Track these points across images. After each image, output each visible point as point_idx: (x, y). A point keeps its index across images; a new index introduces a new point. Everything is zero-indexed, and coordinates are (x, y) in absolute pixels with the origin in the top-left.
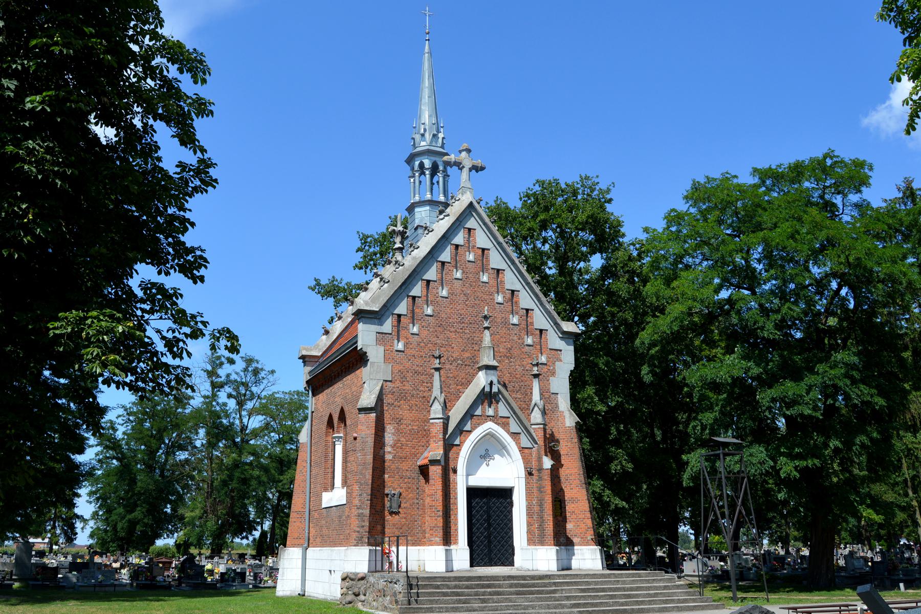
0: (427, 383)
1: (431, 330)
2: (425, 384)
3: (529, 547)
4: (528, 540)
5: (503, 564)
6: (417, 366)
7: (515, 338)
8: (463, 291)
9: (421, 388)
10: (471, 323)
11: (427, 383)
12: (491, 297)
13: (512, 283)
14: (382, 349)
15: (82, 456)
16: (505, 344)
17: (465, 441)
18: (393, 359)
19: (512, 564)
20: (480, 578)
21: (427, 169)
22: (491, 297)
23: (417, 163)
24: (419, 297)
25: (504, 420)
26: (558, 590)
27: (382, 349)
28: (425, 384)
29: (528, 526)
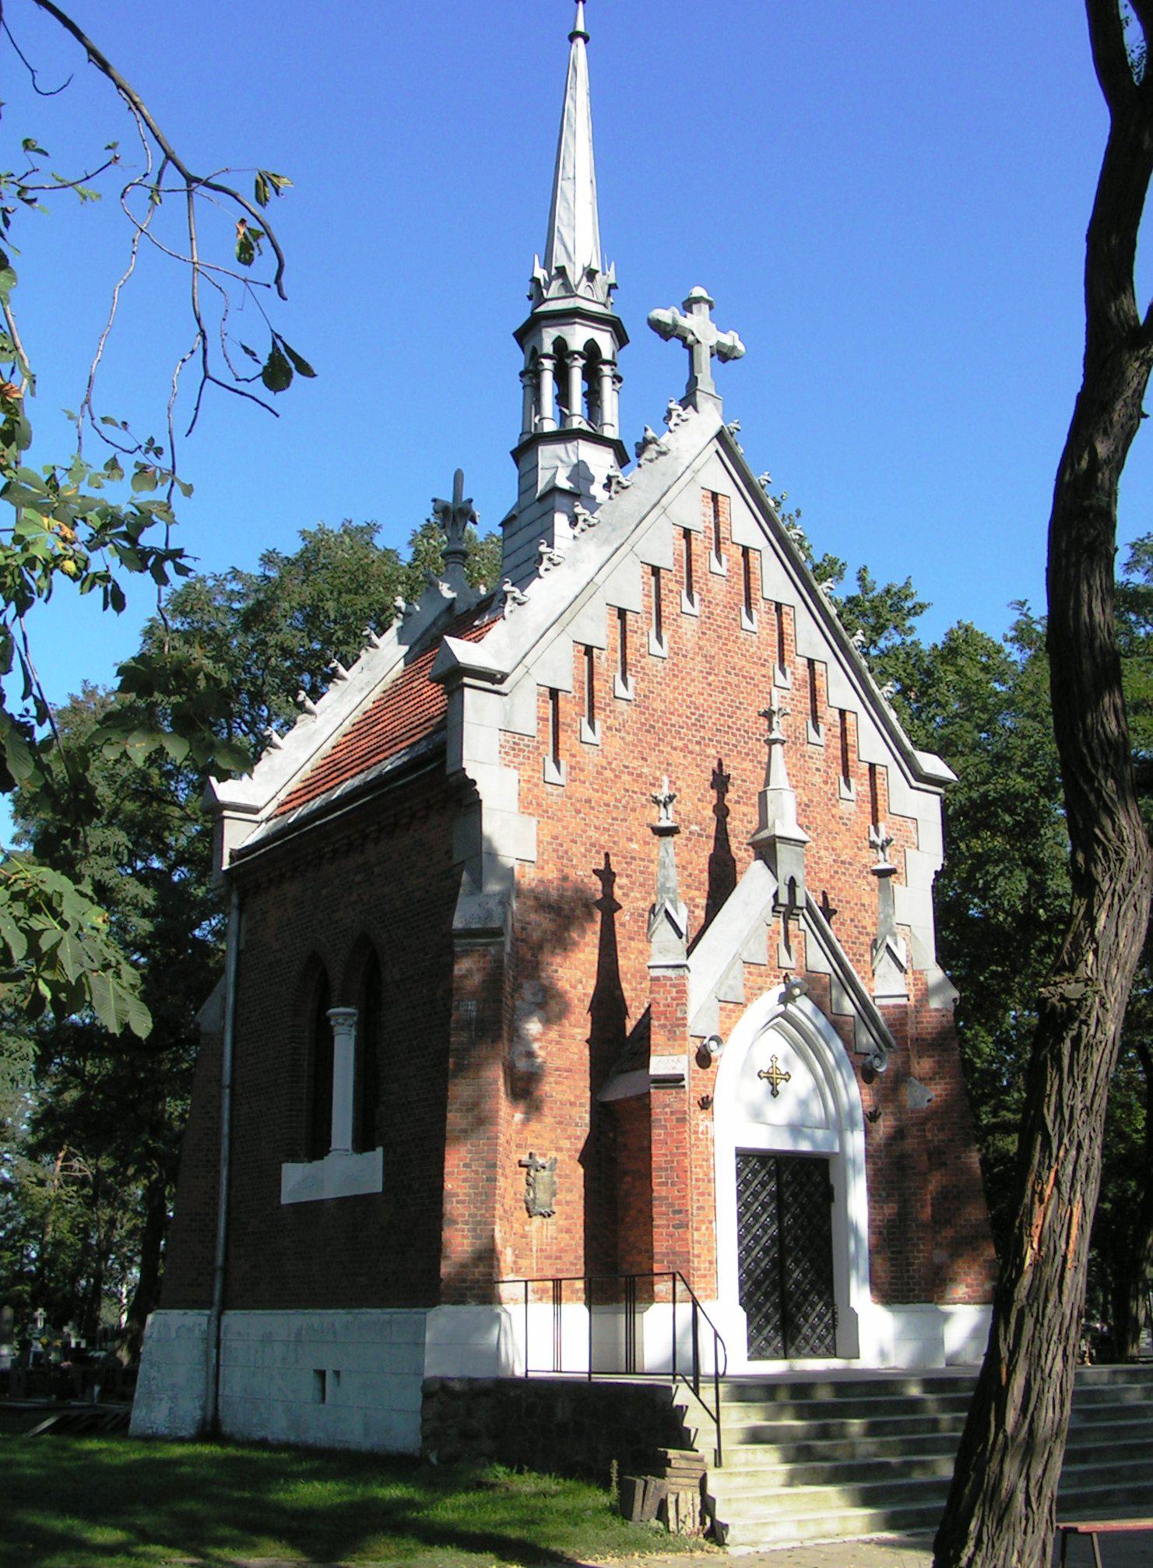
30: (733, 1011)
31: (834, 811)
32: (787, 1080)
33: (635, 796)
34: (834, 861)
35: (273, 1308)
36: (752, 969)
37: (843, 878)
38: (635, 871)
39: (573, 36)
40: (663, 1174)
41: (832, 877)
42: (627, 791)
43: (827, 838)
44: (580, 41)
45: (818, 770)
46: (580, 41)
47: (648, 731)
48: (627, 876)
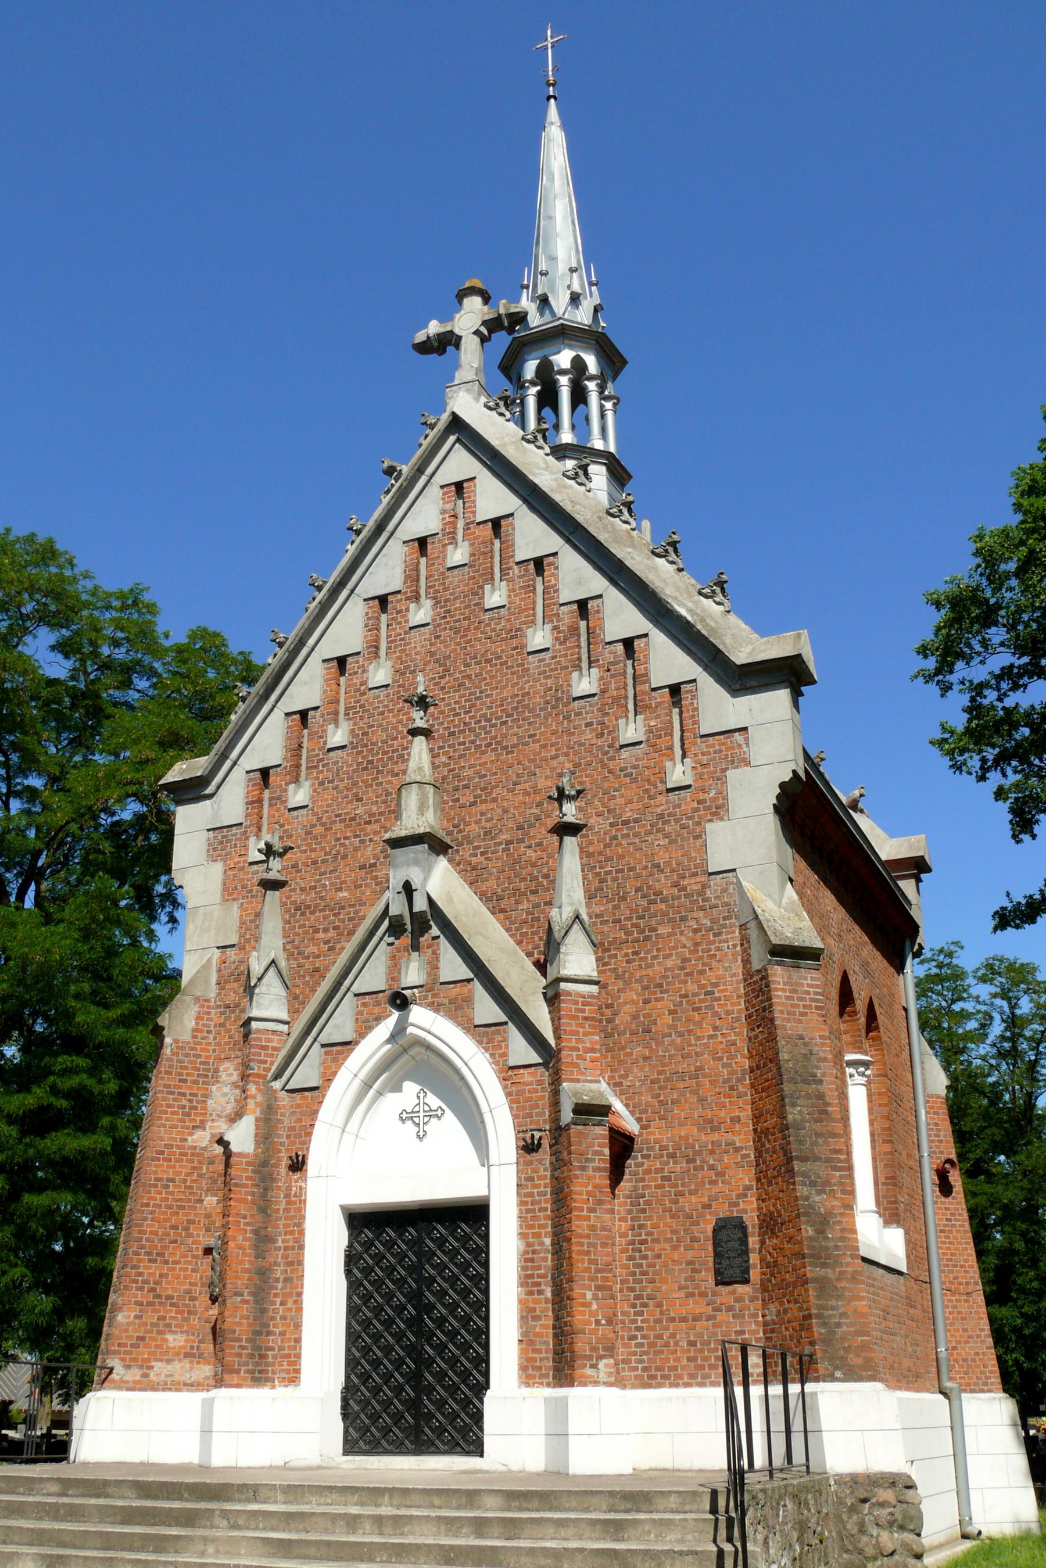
0: (325, 930)
1: (342, 785)
2: (321, 935)
3: (527, 1391)
4: (523, 1368)
5: (454, 1448)
6: (302, 890)
7: (588, 735)
8: (432, 654)
9: (312, 949)
10: (452, 734)
11: (325, 930)
12: (514, 643)
13: (580, 582)
14: (218, 868)
15: (876, 1220)
16: (555, 763)
17: (335, 1073)
18: (244, 887)
19: (477, 1448)
20: (375, 1493)
21: (563, 372)
22: (514, 643)
23: (530, 369)
24: (316, 708)
25: (457, 989)
26: (190, 1539)
27: (218, 868)
28: (321, 935)
29: (523, 1319)
30: (338, 1053)
31: (611, 765)
32: (439, 1118)
33: (347, 842)
34: (612, 825)
35: (99, 1463)
36: (367, 999)
37: (624, 842)
38: (343, 921)
39: (549, 98)
40: (586, 1241)
41: (606, 846)
42: (338, 839)
43: (601, 800)
44: (552, 101)
45: (587, 725)
46: (552, 101)
47: (366, 769)
48: (335, 928)
